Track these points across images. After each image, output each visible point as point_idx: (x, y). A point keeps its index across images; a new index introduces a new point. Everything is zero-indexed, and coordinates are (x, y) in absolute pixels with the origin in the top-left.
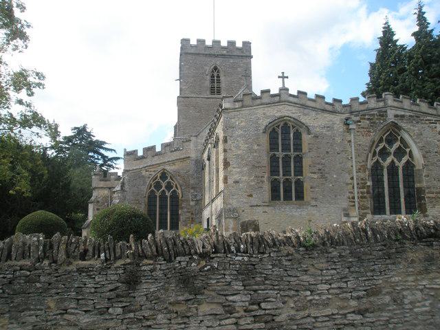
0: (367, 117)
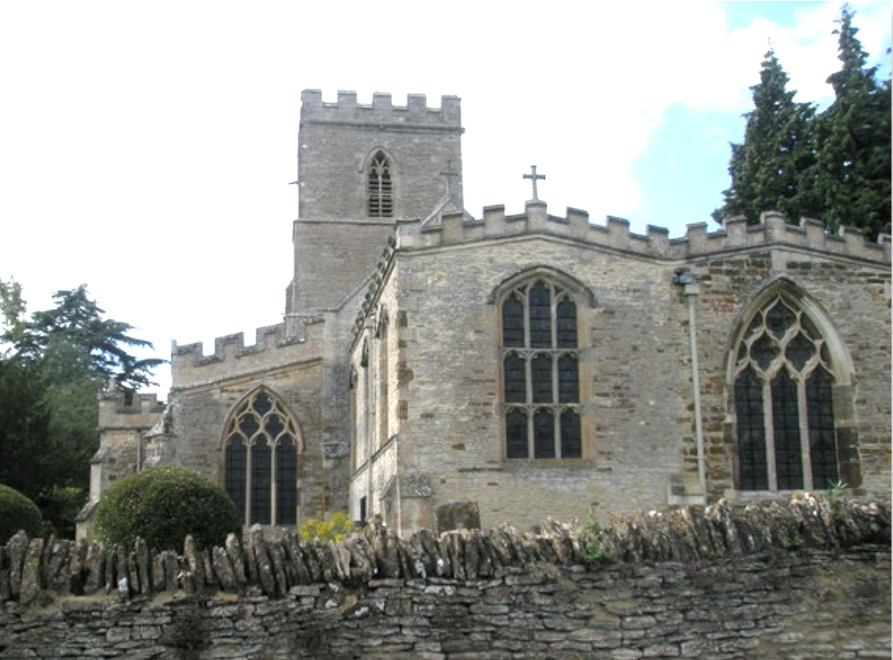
0: (725, 267)
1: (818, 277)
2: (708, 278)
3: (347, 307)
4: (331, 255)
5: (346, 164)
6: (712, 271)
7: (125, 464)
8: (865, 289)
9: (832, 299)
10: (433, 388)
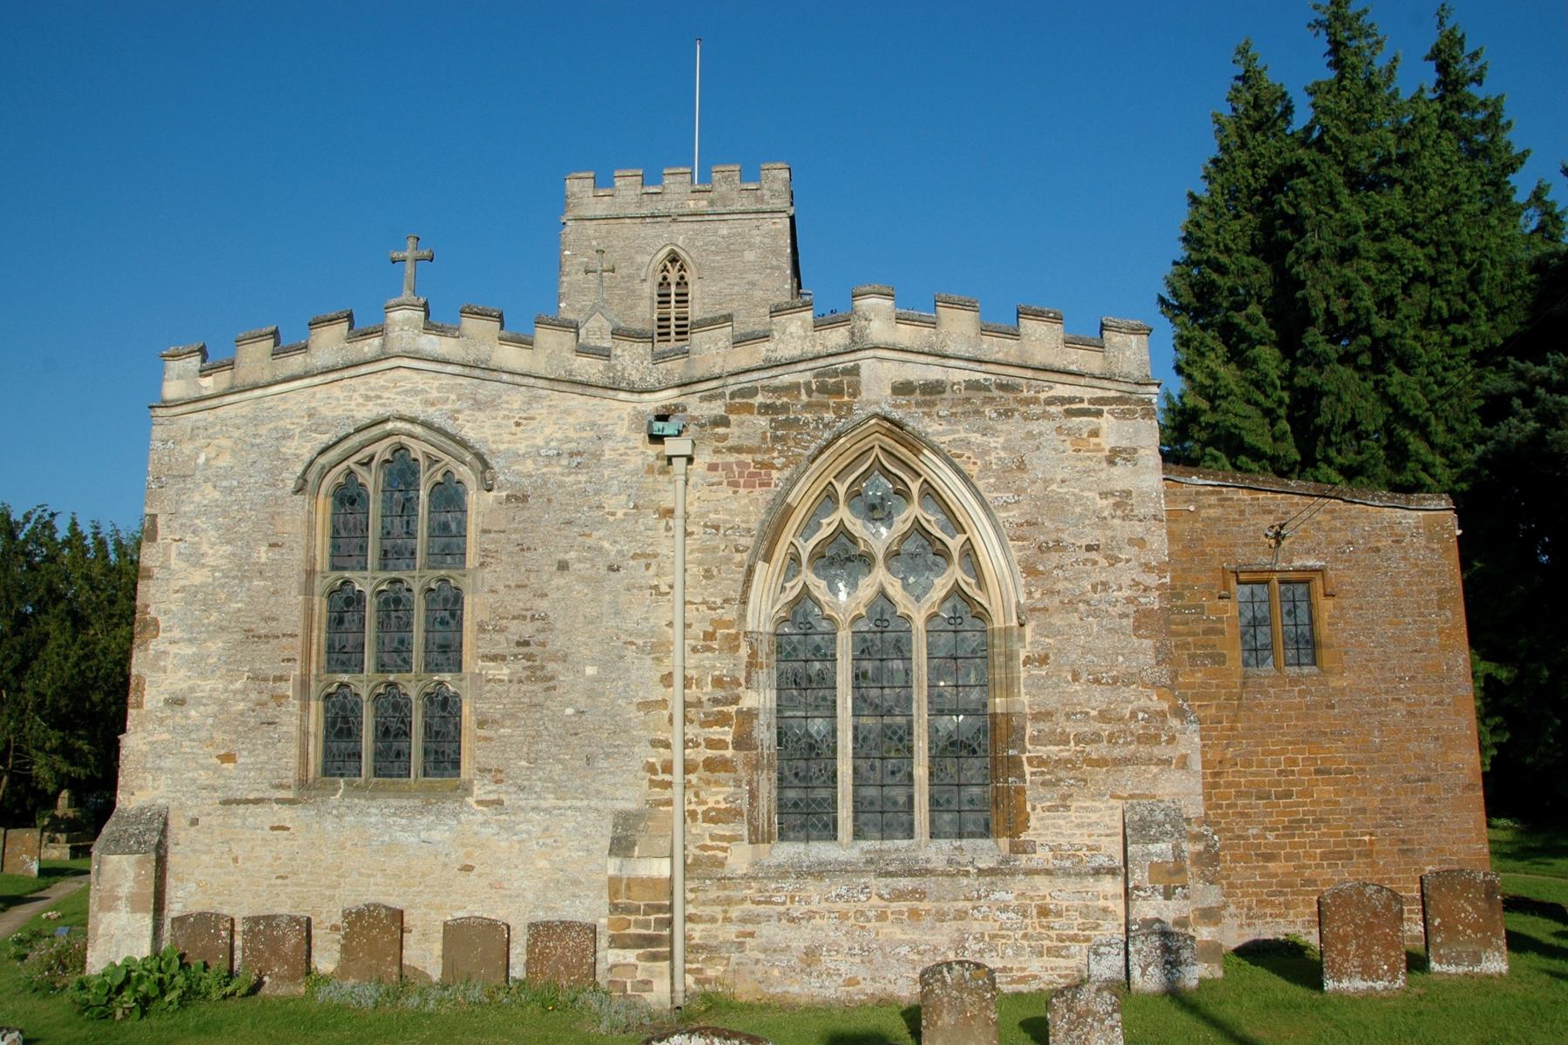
0: (759, 399)
1: (960, 409)
2: (723, 422)
6: (731, 409)
8: (1059, 429)
9: (986, 452)
10: (190, 650)
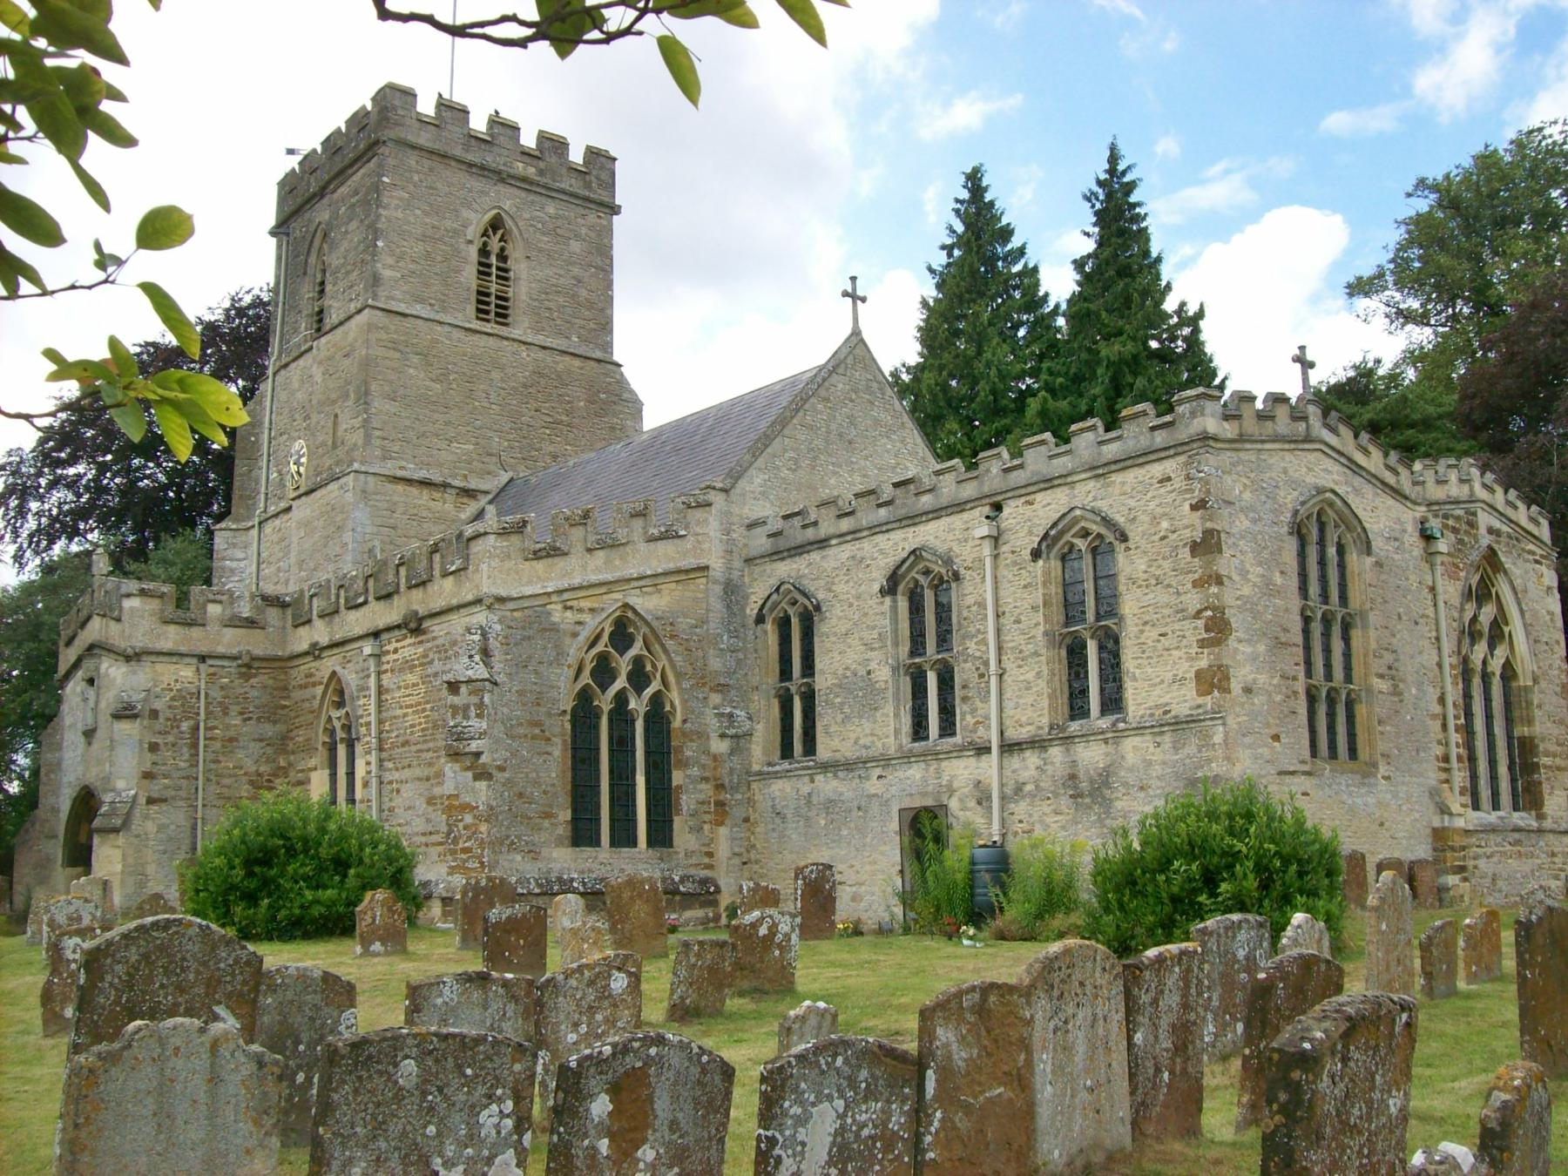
3: (742, 484)
4: (422, 375)
5: (448, 224)
7: (175, 722)
10: (1249, 650)
